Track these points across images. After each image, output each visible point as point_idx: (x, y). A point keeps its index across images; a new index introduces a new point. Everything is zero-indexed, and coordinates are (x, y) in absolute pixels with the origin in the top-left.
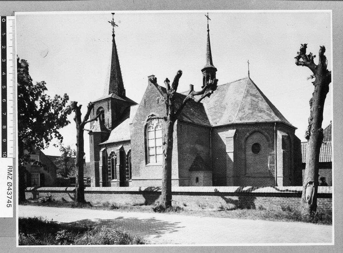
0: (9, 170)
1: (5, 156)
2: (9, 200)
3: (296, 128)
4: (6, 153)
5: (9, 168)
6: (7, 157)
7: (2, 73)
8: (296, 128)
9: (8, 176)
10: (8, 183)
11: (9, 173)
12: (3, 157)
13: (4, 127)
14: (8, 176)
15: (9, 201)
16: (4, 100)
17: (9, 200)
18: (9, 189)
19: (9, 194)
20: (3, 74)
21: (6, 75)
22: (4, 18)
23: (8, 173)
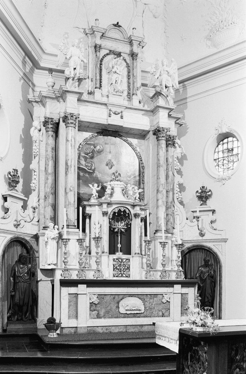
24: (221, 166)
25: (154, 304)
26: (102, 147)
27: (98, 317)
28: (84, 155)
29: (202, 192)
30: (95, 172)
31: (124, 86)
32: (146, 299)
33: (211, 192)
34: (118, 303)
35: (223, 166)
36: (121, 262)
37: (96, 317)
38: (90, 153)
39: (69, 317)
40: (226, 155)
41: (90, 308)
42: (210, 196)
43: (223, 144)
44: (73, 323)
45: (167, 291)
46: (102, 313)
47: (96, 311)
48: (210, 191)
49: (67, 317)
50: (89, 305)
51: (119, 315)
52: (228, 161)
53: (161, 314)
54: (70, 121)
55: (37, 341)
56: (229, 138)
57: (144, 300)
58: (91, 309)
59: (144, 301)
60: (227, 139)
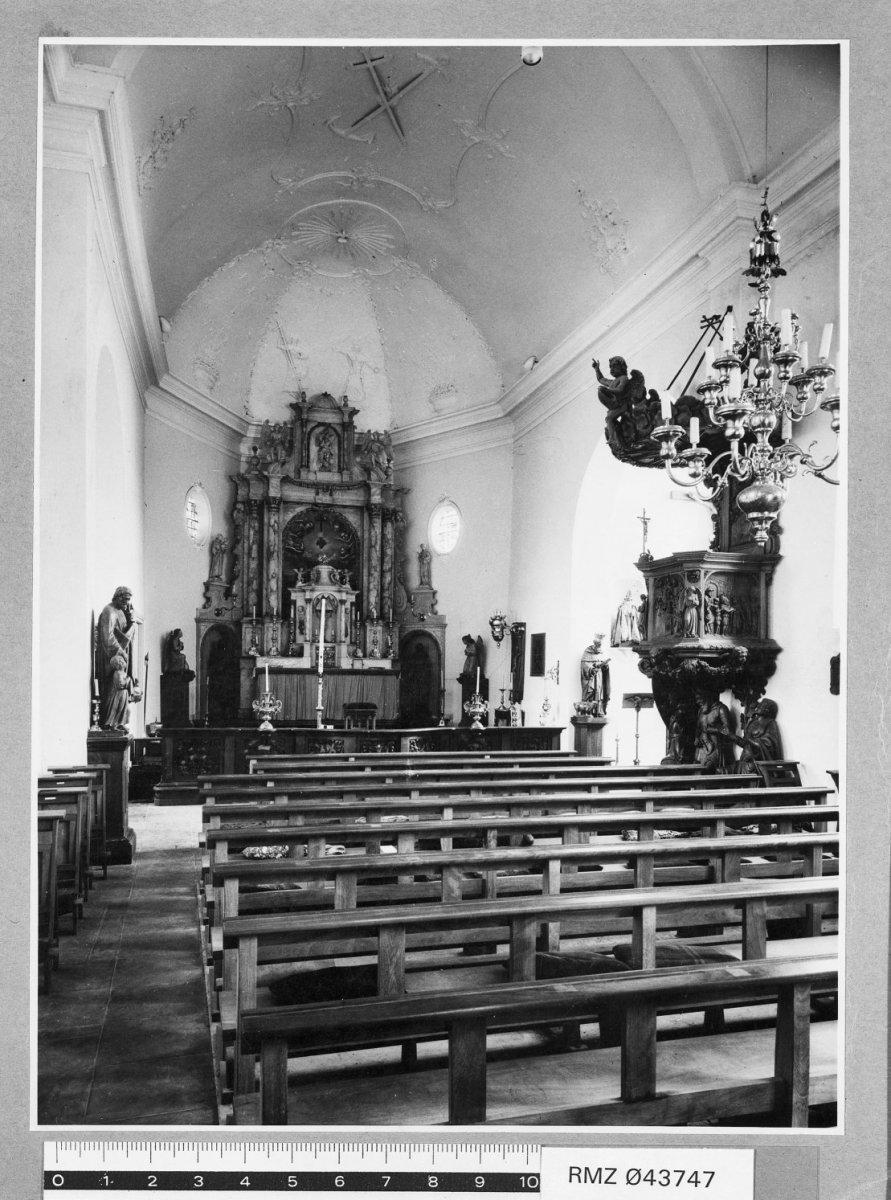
0: (583, 1179)
1: (533, 1182)
2: (689, 1181)
3: (635, 564)
4: (523, 1178)
5: (575, 1178)
6: (538, 1175)
7: (244, 1188)
8: (635, 564)
9: (606, 1182)
10: (629, 1182)
11: (593, 1178)
12: (539, 1186)
13: (433, 1182)
14: (606, 1182)
15: (693, 1179)
16: (340, 1183)
17: (689, 1181)
18: (649, 1178)
19: (666, 1178)
20: (248, 1184)
21: (252, 1175)
22: (49, 1180)
23: (593, 1182)
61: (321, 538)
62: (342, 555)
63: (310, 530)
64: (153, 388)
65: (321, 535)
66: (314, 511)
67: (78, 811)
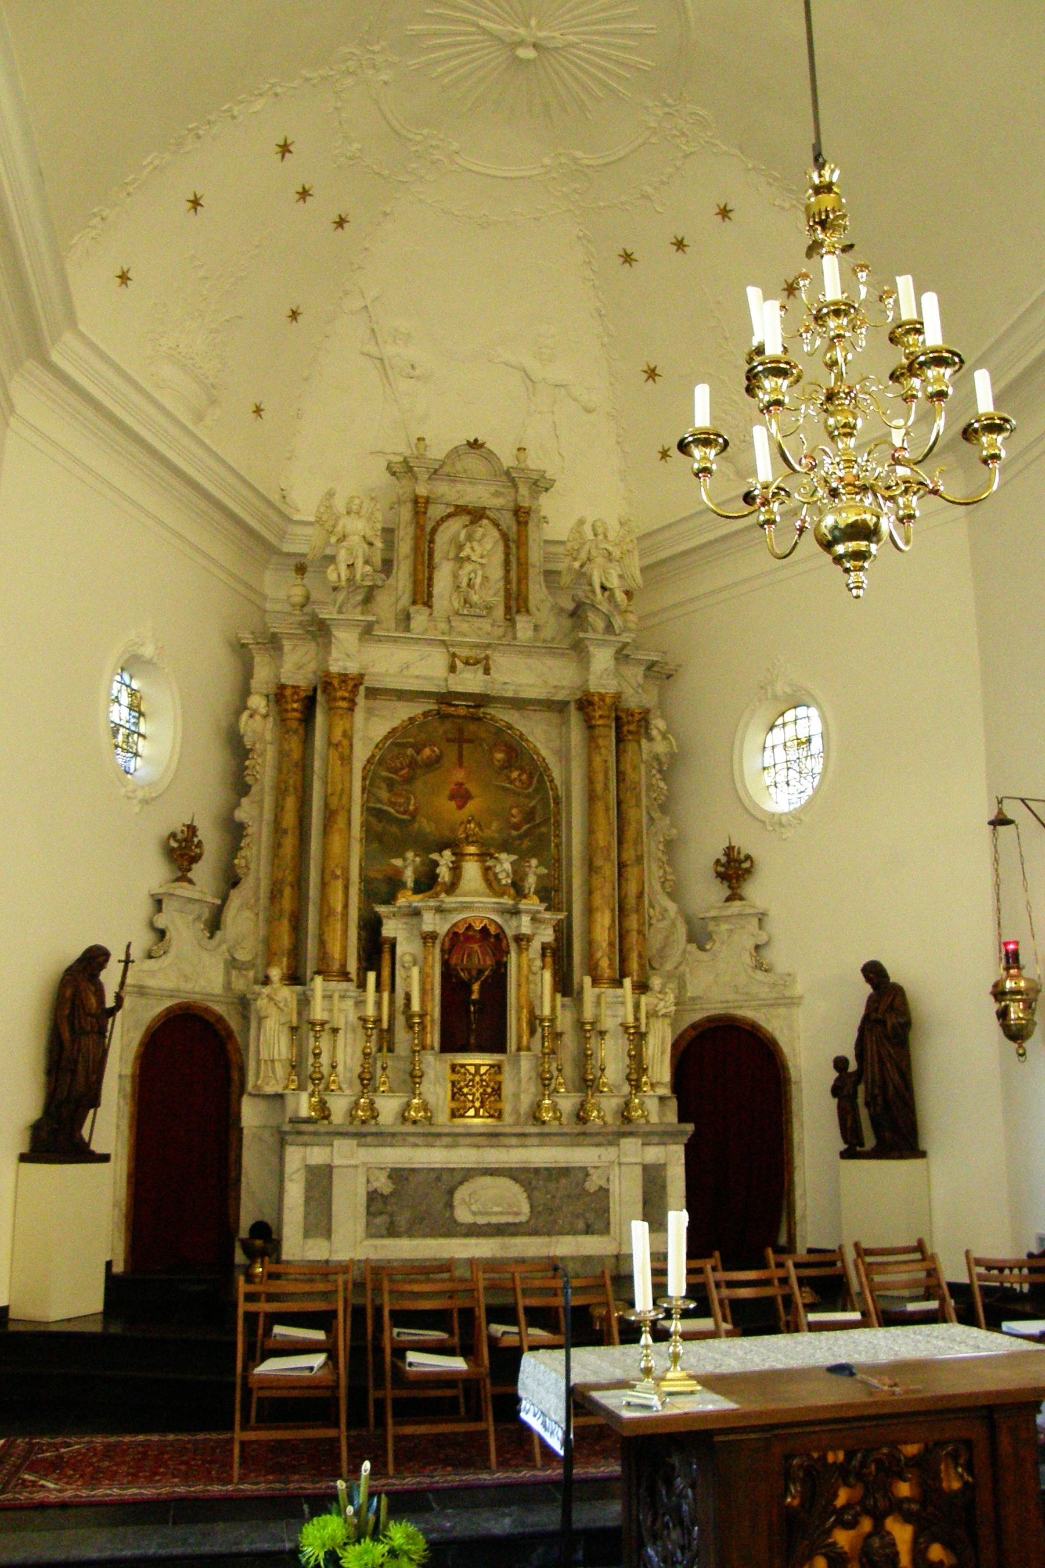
3: (24, 1158)
24: (782, 785)
25: (559, 1195)
26: (436, 749)
27: (392, 1232)
28: (385, 774)
29: (729, 862)
30: (418, 818)
31: (492, 594)
32: (534, 1182)
33: (752, 861)
34: (451, 1192)
35: (788, 784)
36: (474, 1075)
37: (385, 1232)
38: (402, 769)
39: (307, 1234)
40: (793, 755)
41: (368, 1207)
42: (748, 871)
43: (784, 724)
44: (317, 1251)
45: (599, 1157)
46: (402, 1220)
47: (384, 1216)
48: (748, 857)
49: (302, 1231)
50: (362, 1200)
51: (452, 1229)
52: (800, 772)
53: (581, 1225)
54: (339, 694)
55: (832, 1519)
56: (798, 709)
57: (530, 1183)
58: (373, 1209)
59: (529, 1189)
60: (781, 718)
61: (460, 785)
62: (517, 827)
63: (433, 764)
64: (30, 364)
65: (459, 775)
66: (442, 717)
67: (632, 760)
